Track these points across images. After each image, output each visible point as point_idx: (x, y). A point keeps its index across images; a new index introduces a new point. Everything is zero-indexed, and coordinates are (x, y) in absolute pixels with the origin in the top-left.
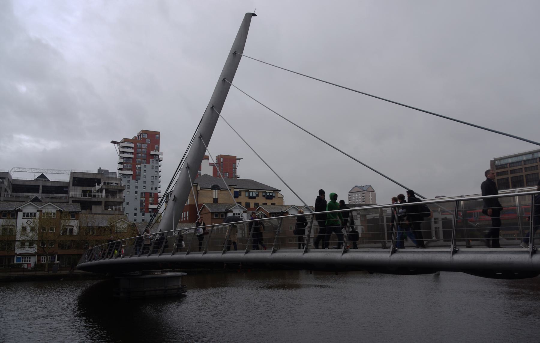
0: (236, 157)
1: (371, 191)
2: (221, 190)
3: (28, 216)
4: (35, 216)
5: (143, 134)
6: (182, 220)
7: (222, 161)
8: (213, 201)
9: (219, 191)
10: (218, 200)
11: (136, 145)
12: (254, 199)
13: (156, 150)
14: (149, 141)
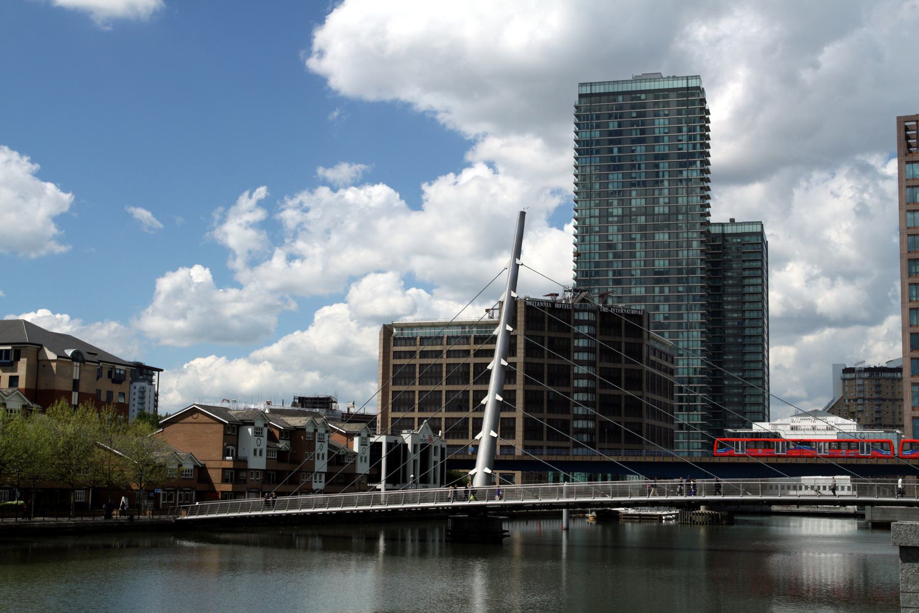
2: (87, 363)
8: (72, 386)
9: (82, 364)
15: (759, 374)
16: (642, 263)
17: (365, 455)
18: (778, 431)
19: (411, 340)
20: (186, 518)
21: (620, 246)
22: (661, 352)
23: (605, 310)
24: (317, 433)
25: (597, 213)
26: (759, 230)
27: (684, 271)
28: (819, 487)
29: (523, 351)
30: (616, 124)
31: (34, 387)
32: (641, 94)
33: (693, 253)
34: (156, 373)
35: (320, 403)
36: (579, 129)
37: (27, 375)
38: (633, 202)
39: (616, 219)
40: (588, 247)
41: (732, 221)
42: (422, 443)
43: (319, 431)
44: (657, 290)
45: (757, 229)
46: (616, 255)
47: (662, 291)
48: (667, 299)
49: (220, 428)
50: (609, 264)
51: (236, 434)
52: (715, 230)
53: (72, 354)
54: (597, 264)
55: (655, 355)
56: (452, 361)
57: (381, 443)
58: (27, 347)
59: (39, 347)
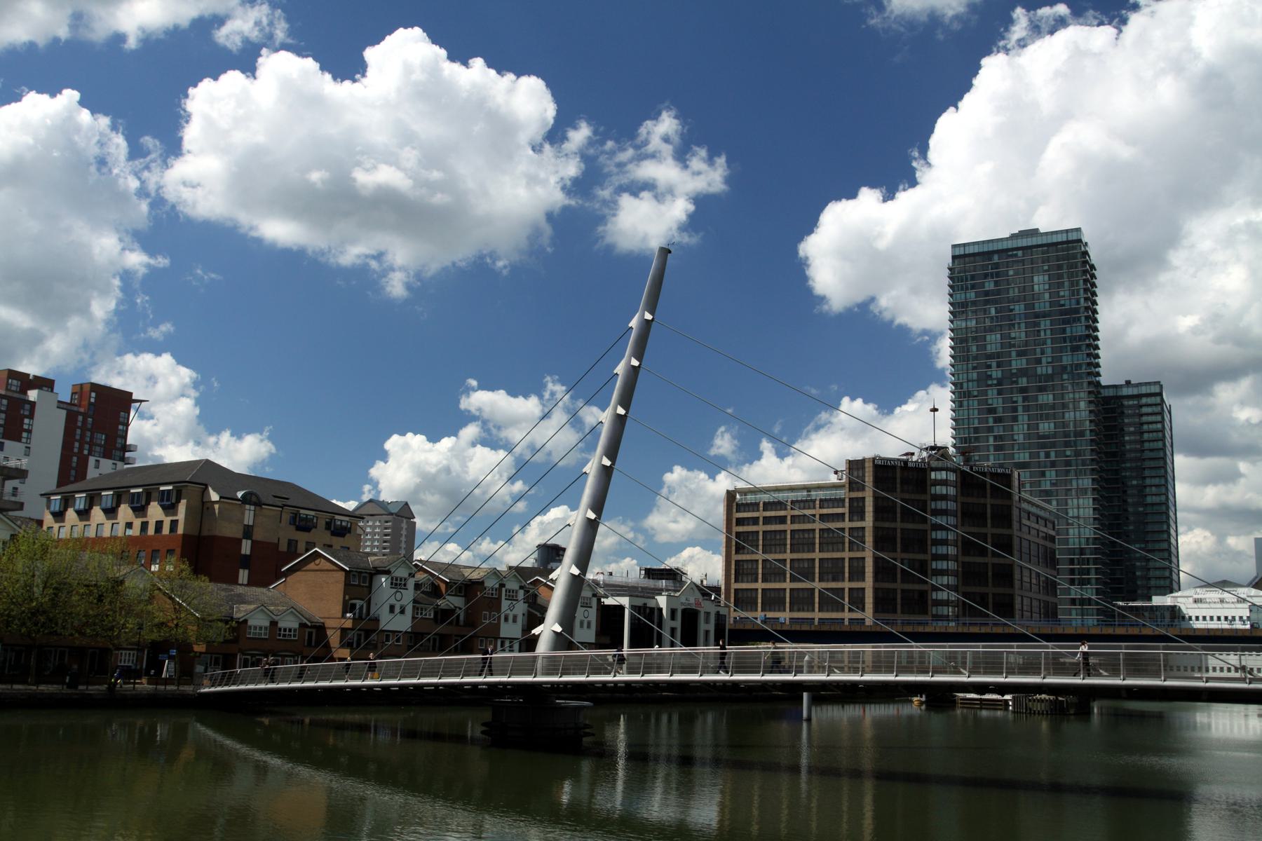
0: (131, 394)
1: (406, 518)
9: (258, 508)
10: (255, 529)
12: (342, 539)
15: (1165, 546)
16: (1026, 426)
17: (589, 619)
18: (1178, 604)
19: (754, 506)
20: (207, 690)
21: (1001, 409)
22: (1038, 517)
23: (967, 469)
24: (504, 589)
25: (975, 376)
26: (1158, 391)
27: (1072, 435)
28: (1252, 669)
31: (197, 534)
33: (1080, 413)
35: (667, 574)
37: (186, 518)
38: (1014, 363)
39: (995, 382)
40: (966, 412)
41: (1128, 383)
42: (683, 607)
43: (507, 587)
44: (1042, 454)
45: (1155, 389)
46: (998, 420)
47: (1048, 455)
48: (1053, 464)
49: (341, 575)
50: (990, 429)
51: (367, 585)
52: (1106, 393)
54: (976, 430)
55: (1029, 519)
58: (187, 486)
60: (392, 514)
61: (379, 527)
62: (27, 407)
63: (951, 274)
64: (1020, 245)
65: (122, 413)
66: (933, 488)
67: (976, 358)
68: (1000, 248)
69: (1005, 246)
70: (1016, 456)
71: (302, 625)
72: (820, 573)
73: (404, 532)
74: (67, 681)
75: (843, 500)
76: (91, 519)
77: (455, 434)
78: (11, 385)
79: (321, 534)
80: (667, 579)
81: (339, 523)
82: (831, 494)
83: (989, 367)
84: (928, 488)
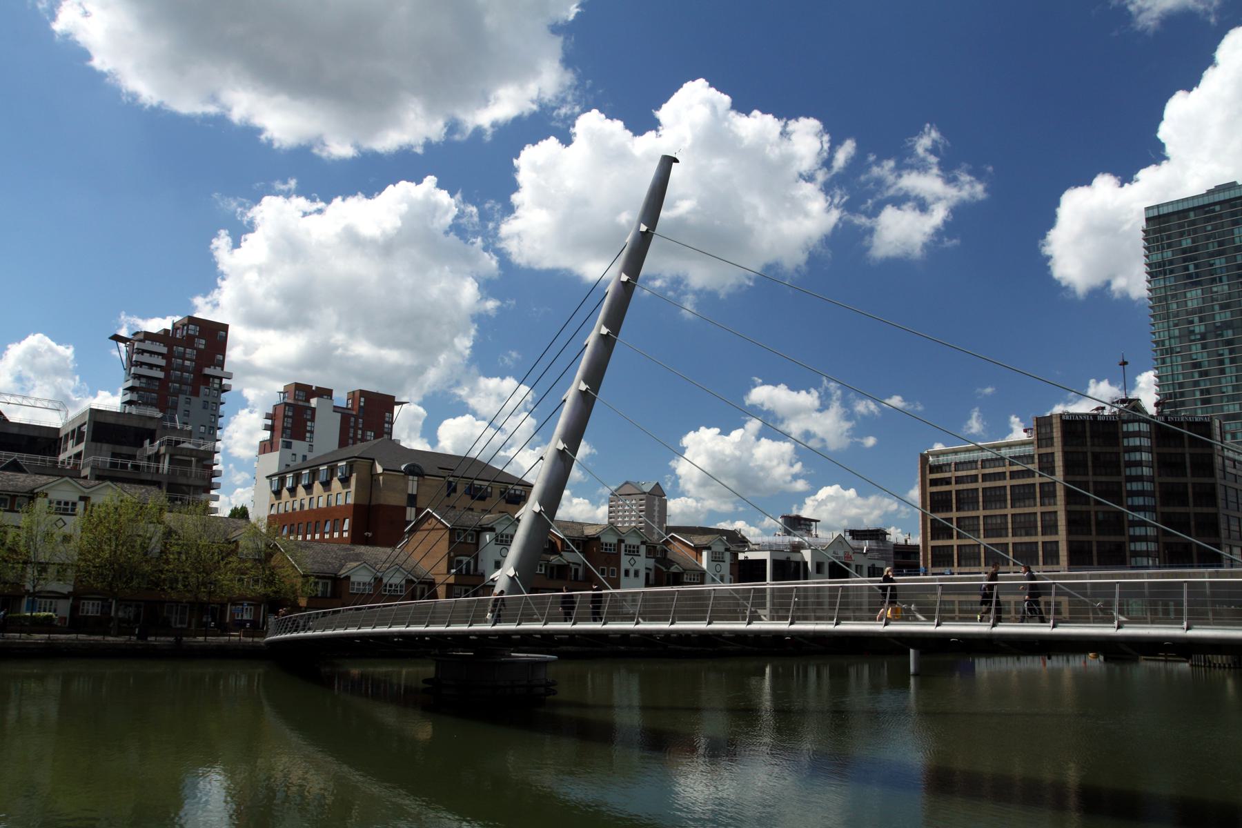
0: (394, 397)
1: (658, 496)
2: (426, 477)
3: (502, 541)
4: (73, 510)
5: (190, 326)
6: (327, 536)
7: (362, 404)
9: (421, 478)
11: (170, 350)
13: (215, 366)
14: (201, 343)
16: (1234, 378)
21: (1206, 363)
24: (623, 545)
25: (1177, 333)
29: (1062, 469)
30: (1189, 241)
31: (367, 503)
32: (1214, 205)
34: (814, 523)
35: (870, 535)
36: (1149, 252)
39: (1198, 337)
40: (1170, 369)
43: (626, 542)
46: (1202, 374)
50: (1196, 384)
53: (405, 468)
54: (1181, 385)
56: (988, 484)
57: (765, 561)
58: (356, 461)
59: (371, 461)
60: (645, 493)
61: (635, 504)
62: (309, 412)
63: (1146, 236)
64: (1217, 200)
65: (387, 414)
66: (1125, 441)
67: (1177, 315)
68: (1196, 205)
69: (1201, 202)
70: (1226, 408)
71: (409, 582)
72: (1012, 529)
73: (656, 508)
74: (137, 632)
75: (1032, 457)
76: (298, 495)
77: (743, 427)
78: (298, 395)
79: (495, 501)
80: (870, 539)
81: (513, 492)
82: (1024, 451)
83: (1192, 322)
84: (1121, 440)
